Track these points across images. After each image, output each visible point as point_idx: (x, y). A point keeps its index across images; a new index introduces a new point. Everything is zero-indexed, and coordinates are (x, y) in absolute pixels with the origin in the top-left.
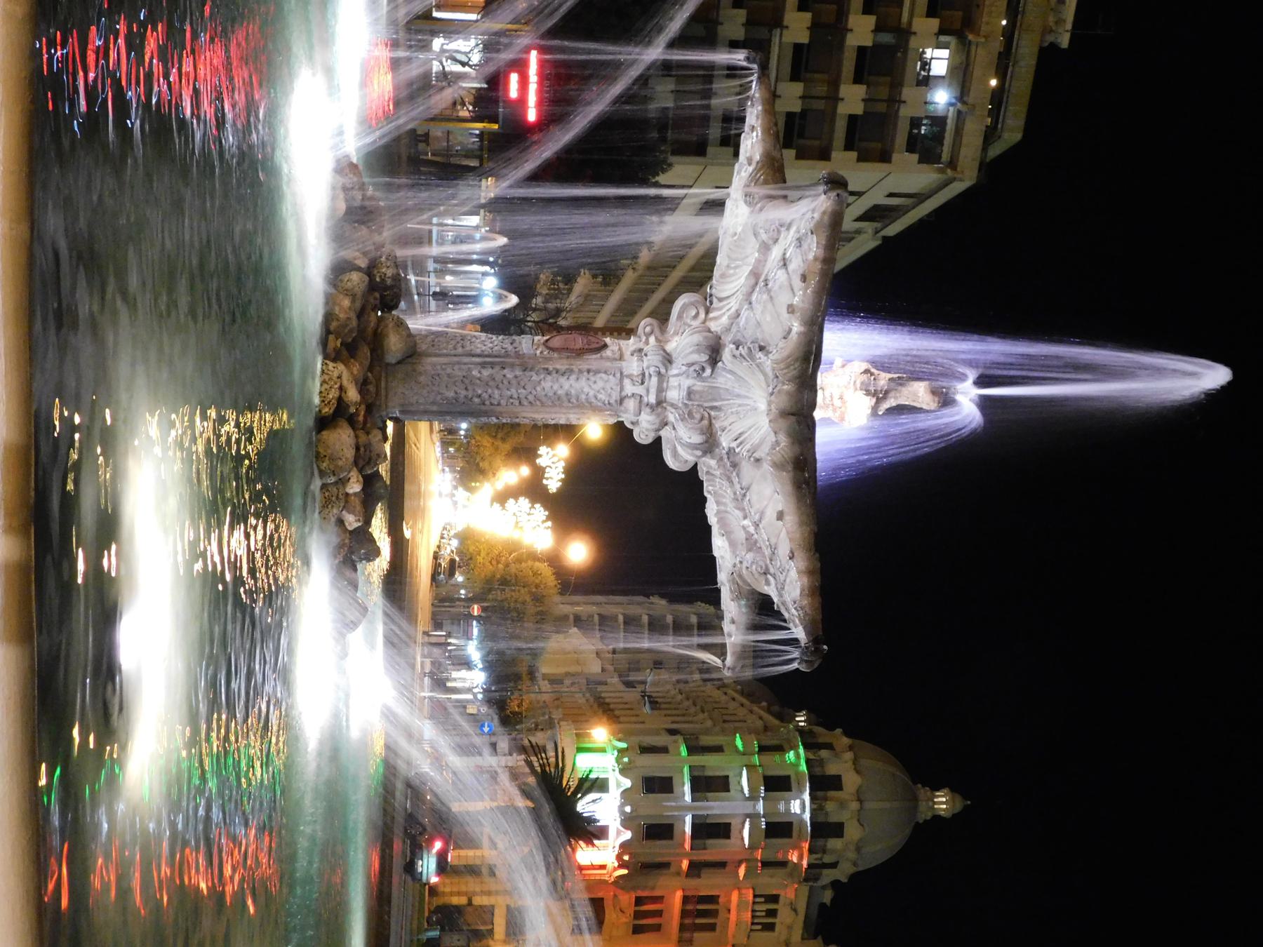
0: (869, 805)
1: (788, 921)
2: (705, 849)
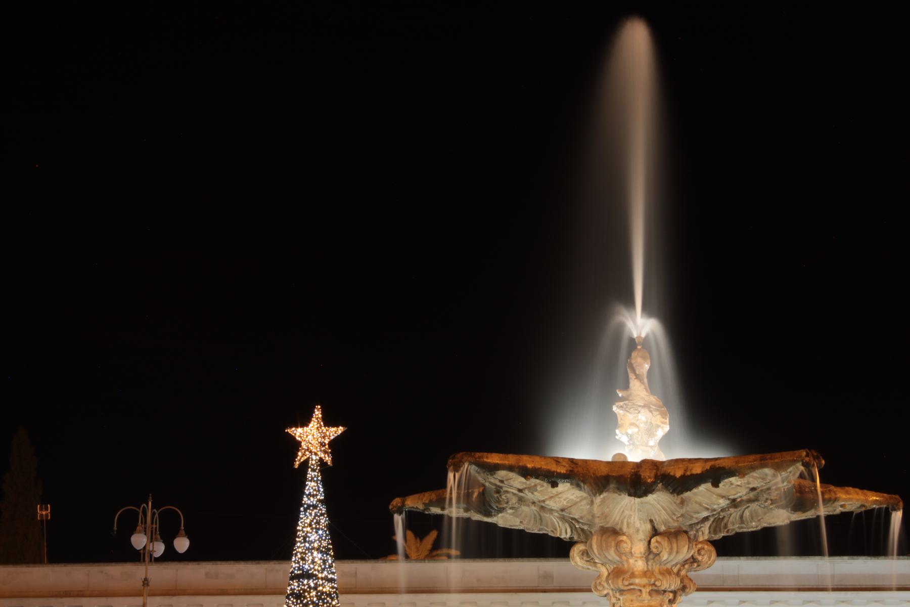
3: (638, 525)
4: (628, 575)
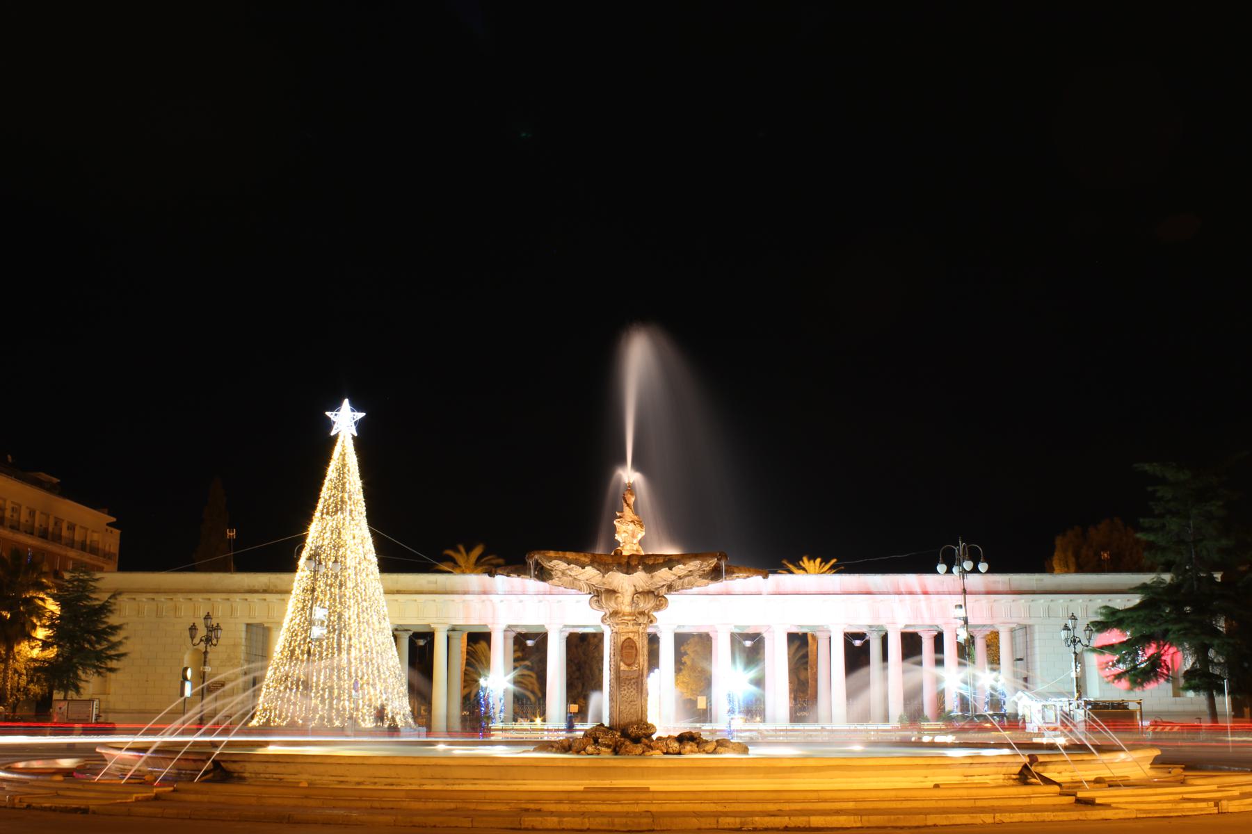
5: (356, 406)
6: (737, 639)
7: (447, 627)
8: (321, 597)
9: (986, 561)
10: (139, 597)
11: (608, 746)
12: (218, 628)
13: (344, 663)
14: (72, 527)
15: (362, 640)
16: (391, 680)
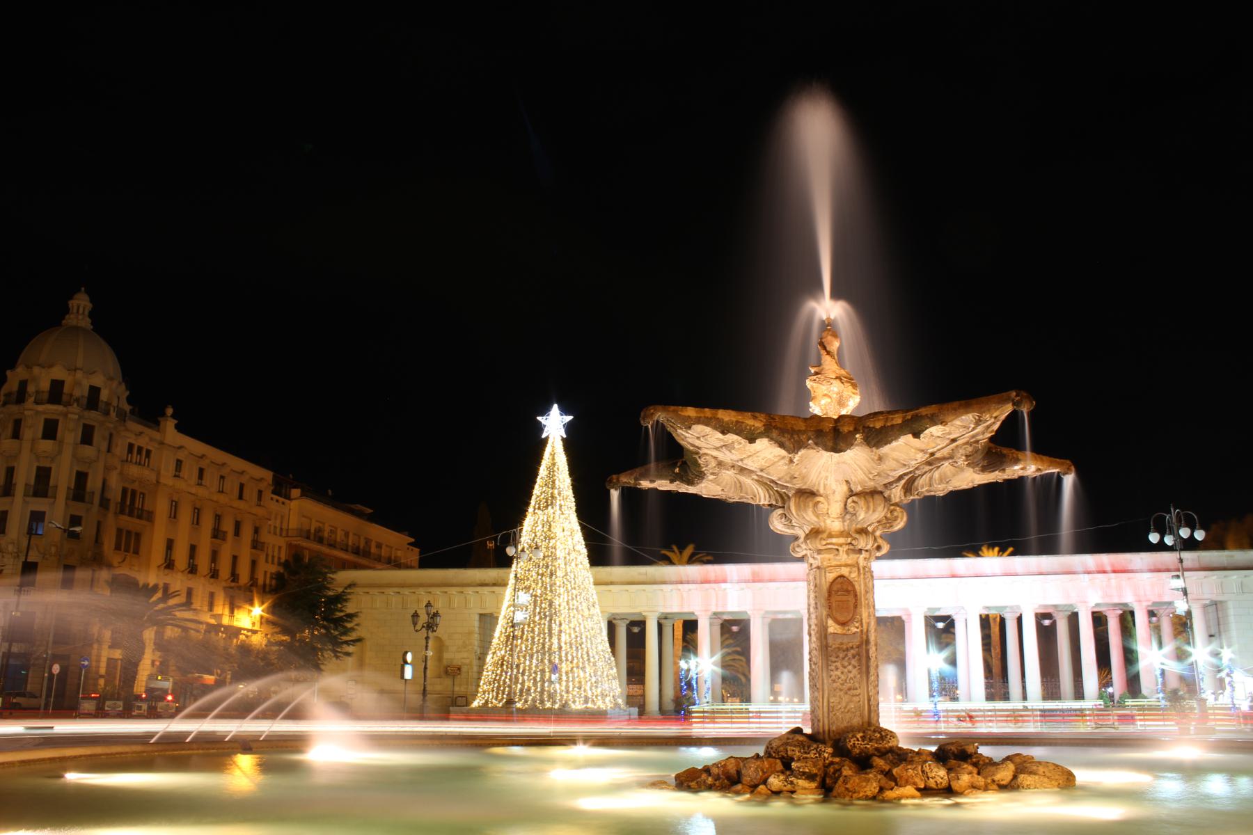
0: (80, 364)
1: (147, 439)
2: (56, 487)
3: (834, 487)
4: (825, 536)
5: (564, 410)
6: (931, 620)
7: (657, 615)
8: (533, 585)
9: (1202, 528)
10: (387, 591)
11: (810, 777)
12: (436, 615)
13: (555, 646)
14: (379, 546)
15: (572, 625)
16: (600, 664)
